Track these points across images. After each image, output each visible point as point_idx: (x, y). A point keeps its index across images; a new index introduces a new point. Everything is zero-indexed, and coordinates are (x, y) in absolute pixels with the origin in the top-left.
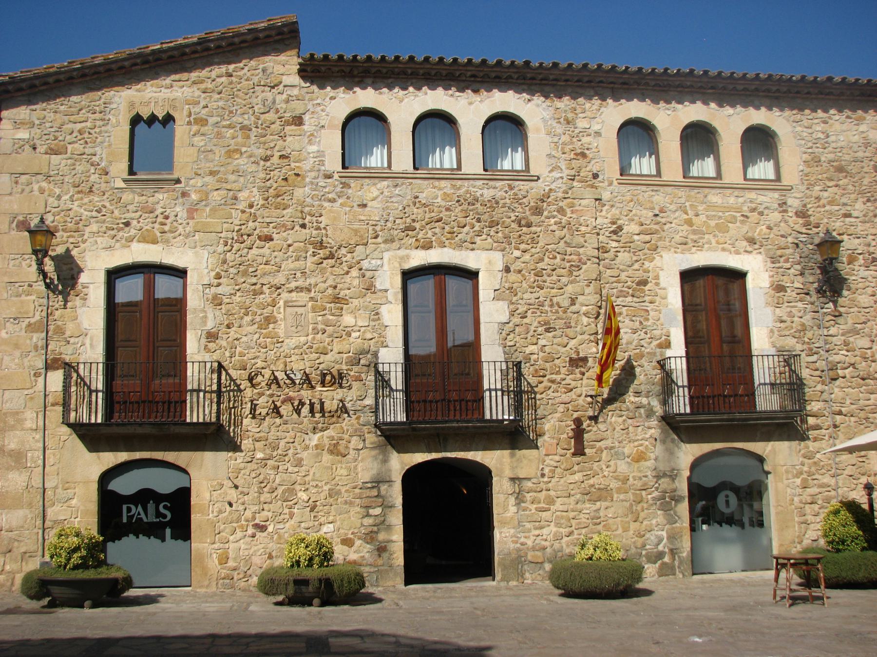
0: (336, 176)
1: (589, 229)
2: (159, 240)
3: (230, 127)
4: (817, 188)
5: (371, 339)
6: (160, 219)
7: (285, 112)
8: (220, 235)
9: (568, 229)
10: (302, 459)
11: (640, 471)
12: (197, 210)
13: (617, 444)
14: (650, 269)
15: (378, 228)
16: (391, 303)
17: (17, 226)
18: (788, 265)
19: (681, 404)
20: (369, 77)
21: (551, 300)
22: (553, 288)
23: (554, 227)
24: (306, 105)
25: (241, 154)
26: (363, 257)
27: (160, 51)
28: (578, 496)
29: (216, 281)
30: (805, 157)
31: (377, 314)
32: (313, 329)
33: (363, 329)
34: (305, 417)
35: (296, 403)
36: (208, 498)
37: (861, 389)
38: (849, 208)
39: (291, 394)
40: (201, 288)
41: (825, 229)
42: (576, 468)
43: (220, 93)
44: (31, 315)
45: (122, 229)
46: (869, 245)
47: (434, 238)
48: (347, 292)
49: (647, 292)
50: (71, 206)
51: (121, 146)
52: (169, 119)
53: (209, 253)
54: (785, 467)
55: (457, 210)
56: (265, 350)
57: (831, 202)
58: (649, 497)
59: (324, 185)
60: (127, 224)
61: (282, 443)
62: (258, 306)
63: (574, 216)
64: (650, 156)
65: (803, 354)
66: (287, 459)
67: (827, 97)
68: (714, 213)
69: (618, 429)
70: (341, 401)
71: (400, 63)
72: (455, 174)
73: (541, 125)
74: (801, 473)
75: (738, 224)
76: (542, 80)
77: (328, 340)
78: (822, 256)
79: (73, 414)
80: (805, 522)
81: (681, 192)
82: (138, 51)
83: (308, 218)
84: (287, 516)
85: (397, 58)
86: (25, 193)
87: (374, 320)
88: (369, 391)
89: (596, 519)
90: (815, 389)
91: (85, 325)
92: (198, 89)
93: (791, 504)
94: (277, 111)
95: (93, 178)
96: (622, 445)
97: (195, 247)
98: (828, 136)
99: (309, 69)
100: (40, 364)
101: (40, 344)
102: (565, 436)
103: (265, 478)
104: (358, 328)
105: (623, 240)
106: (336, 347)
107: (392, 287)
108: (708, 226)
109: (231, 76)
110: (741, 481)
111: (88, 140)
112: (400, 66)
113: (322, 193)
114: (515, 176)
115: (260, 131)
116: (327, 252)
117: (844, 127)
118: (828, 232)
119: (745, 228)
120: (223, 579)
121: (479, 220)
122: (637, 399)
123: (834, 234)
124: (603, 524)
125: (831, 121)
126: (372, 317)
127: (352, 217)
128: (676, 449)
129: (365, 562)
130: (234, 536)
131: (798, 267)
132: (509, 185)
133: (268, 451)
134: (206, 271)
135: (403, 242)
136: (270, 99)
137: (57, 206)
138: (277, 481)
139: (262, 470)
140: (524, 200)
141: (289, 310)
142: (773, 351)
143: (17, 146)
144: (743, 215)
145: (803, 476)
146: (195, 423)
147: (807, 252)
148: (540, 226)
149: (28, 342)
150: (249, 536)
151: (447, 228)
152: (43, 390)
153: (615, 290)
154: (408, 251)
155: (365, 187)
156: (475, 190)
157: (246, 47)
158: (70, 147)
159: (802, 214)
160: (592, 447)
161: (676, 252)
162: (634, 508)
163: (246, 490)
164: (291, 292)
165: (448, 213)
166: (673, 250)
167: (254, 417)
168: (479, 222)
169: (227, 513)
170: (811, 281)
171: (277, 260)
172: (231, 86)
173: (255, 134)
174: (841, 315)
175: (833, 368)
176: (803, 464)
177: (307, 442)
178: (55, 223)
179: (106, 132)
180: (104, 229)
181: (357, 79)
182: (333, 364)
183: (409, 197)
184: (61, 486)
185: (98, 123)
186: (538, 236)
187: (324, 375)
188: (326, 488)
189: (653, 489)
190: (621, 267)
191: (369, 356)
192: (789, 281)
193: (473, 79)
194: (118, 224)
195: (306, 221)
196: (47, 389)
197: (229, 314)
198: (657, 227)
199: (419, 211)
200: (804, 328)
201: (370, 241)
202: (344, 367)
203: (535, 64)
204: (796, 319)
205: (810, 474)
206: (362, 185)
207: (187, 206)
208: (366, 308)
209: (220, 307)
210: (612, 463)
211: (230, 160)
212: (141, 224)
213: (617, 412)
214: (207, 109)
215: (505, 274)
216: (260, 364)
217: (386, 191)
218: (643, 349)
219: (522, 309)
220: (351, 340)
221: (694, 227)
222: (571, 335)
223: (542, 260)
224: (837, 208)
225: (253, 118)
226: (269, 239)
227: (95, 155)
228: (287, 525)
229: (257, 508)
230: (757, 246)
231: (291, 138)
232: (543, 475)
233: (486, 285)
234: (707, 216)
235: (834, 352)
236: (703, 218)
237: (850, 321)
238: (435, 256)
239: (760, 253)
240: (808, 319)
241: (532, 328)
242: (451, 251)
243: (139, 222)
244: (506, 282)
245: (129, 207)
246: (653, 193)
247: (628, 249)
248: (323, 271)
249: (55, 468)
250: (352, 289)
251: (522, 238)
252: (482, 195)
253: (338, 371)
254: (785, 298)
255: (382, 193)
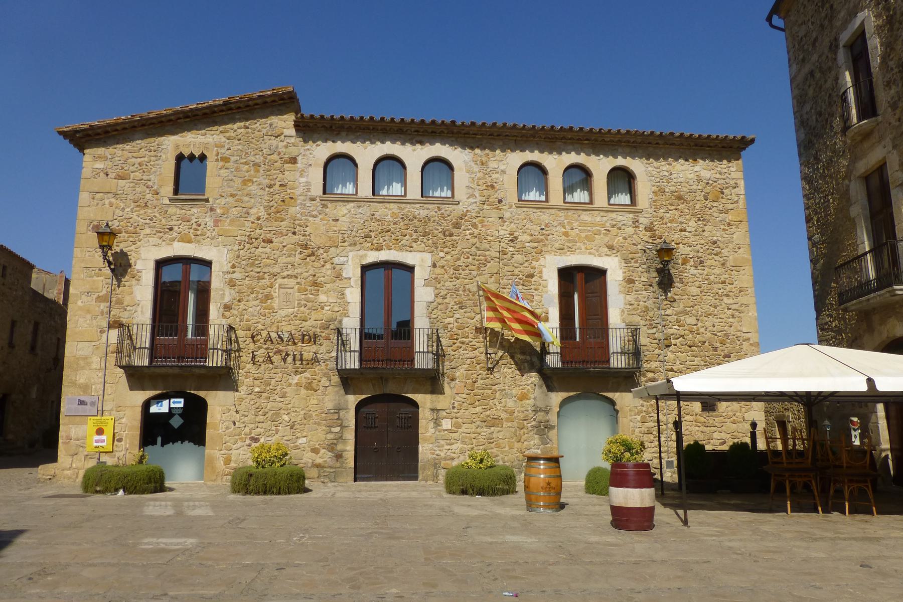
0: (318, 200)
1: (494, 238)
2: (193, 240)
3: (246, 163)
4: (662, 211)
6: (194, 226)
7: (284, 154)
8: (236, 238)
9: (479, 238)
11: (523, 407)
12: (220, 221)
13: (507, 387)
14: (536, 266)
15: (346, 236)
16: (353, 287)
17: (93, 228)
18: (637, 265)
21: (464, 287)
22: (466, 279)
23: (469, 237)
24: (300, 150)
25: (253, 183)
26: (334, 255)
27: (197, 109)
28: (478, 423)
30: (654, 188)
31: (343, 294)
32: (298, 304)
33: (332, 305)
34: (290, 363)
35: (284, 354)
36: (219, 419)
37: (688, 354)
38: (684, 225)
42: (477, 403)
43: (239, 140)
45: (167, 232)
46: (698, 252)
47: (384, 244)
49: (533, 283)
50: (131, 216)
52: (203, 157)
54: (629, 408)
57: (671, 221)
58: (529, 425)
59: (310, 205)
61: (273, 382)
62: (261, 288)
64: (536, 192)
66: (276, 392)
67: (671, 146)
68: (584, 228)
69: (508, 377)
70: (315, 353)
72: (400, 200)
76: (465, 134)
81: (561, 213)
82: (180, 109)
83: (298, 227)
84: (274, 432)
85: (362, 118)
89: (490, 440)
90: (654, 353)
96: (510, 388)
98: (671, 174)
99: (301, 125)
100: (105, 324)
103: (260, 405)
108: (580, 237)
111: (145, 170)
112: (364, 123)
114: (444, 201)
115: (266, 167)
116: (310, 251)
119: (607, 239)
121: (416, 232)
124: (495, 443)
129: (326, 465)
131: (645, 266)
133: (263, 387)
135: (363, 245)
138: (268, 408)
142: (623, 325)
144: (606, 230)
149: (97, 309)
151: (394, 237)
153: (510, 281)
154: (366, 252)
155: (338, 207)
156: (414, 210)
157: (259, 108)
158: (132, 175)
159: (649, 229)
161: (555, 255)
162: (518, 432)
163: (246, 414)
165: (395, 226)
166: (553, 253)
167: (254, 364)
168: (416, 233)
169: (232, 429)
171: (275, 256)
172: (247, 135)
173: (263, 169)
174: (675, 301)
177: (291, 381)
178: (120, 227)
180: (154, 232)
181: (335, 132)
183: (368, 215)
184: (115, 409)
185: (153, 158)
186: (457, 243)
187: (304, 336)
188: (302, 412)
189: (532, 420)
190: (515, 265)
191: (336, 323)
192: (637, 276)
193: (416, 133)
195: (296, 230)
198: (542, 237)
199: (375, 224)
200: (647, 309)
201: (340, 244)
203: (459, 123)
204: (641, 303)
207: (214, 218)
210: (503, 400)
211: (245, 187)
212: (180, 229)
213: (508, 365)
216: (260, 327)
217: (352, 210)
219: (443, 293)
220: (324, 312)
221: (570, 238)
223: (459, 259)
224: (675, 225)
227: (150, 181)
230: (614, 251)
231: (288, 172)
232: (454, 408)
233: (420, 276)
234: (580, 230)
236: (577, 231)
237: (682, 305)
239: (617, 256)
240: (650, 303)
241: (450, 306)
242: (395, 252)
243: (179, 228)
244: (433, 274)
245: (172, 217)
246: (541, 214)
248: (306, 264)
250: (326, 277)
252: (419, 214)
253: (314, 332)
254: (634, 288)
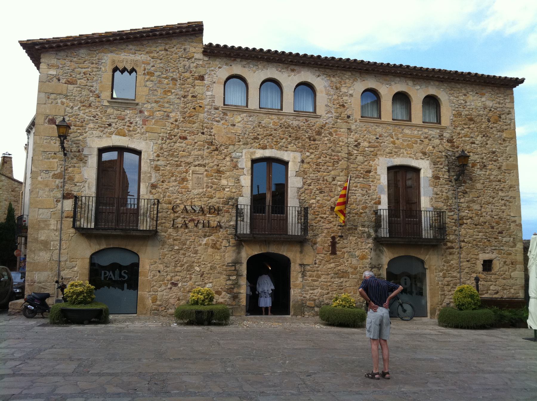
0: (220, 109)
2: (127, 135)
3: (166, 78)
4: (459, 128)
5: (235, 192)
6: (128, 124)
7: (195, 73)
10: (198, 250)
13: (352, 250)
14: (373, 165)
17: (49, 121)
18: (442, 166)
19: (384, 232)
20: (239, 58)
21: (323, 178)
22: (324, 172)
23: (326, 142)
28: (332, 275)
29: (157, 158)
31: (238, 180)
32: (206, 186)
33: (231, 187)
34: (201, 229)
35: (196, 222)
38: (474, 139)
39: (194, 217)
40: (149, 161)
41: (462, 149)
42: (332, 261)
44: (55, 169)
45: (107, 127)
47: (268, 144)
48: (224, 168)
50: (79, 113)
51: (107, 83)
53: (154, 144)
55: (280, 131)
56: (181, 195)
57: (465, 136)
59: (214, 113)
60: (110, 125)
61: (188, 242)
62: (178, 172)
63: (337, 137)
65: (447, 211)
69: (353, 243)
70: (219, 222)
71: (255, 52)
73: (324, 89)
74: (443, 270)
75: (418, 145)
76: (325, 66)
77: (213, 192)
78: (459, 163)
79: (78, 223)
80: (444, 294)
83: (206, 129)
84: (189, 279)
86: (53, 104)
87: (236, 183)
88: (233, 218)
89: (340, 287)
91: (86, 176)
92: (149, 56)
93: (437, 285)
94: (191, 72)
95: (91, 99)
96: (355, 251)
97: (146, 140)
100: (60, 195)
101: (60, 185)
102: (327, 245)
103: (179, 259)
104: (228, 187)
105: (360, 150)
106: (217, 196)
107: (246, 167)
108: (403, 145)
109: (167, 51)
110: (413, 273)
111: (89, 78)
113: (213, 117)
116: (214, 147)
117: (475, 98)
118: (463, 151)
119: (421, 147)
120: (154, 310)
121: (290, 136)
122: (363, 229)
123: (466, 152)
125: (468, 95)
126: (236, 181)
127: (227, 130)
128: (381, 254)
130: (161, 288)
132: (306, 120)
133: (180, 246)
134: (152, 153)
135: (253, 145)
136: (188, 65)
137: (71, 112)
139: (177, 255)
140: (313, 128)
141: (194, 175)
142: (431, 209)
143: (49, 78)
144: (420, 140)
145: (443, 272)
146: (144, 230)
147: (451, 160)
148: (320, 141)
149: (53, 183)
150: (168, 289)
151: (275, 140)
152: (61, 209)
153: (355, 175)
154: (255, 150)
155: (235, 116)
159: (450, 141)
160: (340, 251)
161: (386, 157)
164: (195, 166)
165: (275, 132)
166: (384, 156)
170: (453, 175)
171: (189, 150)
173: (179, 83)
175: (462, 218)
176: (444, 266)
178: (70, 122)
179: (99, 75)
180: (97, 127)
181: (232, 59)
182: (215, 204)
183: (256, 123)
184: (69, 260)
185: (95, 70)
187: (210, 209)
190: (358, 163)
191: (233, 200)
194: (105, 124)
195: (204, 131)
196: (63, 209)
197: (163, 175)
198: (377, 144)
200: (448, 198)
202: (221, 205)
205: (447, 271)
206: (233, 114)
208: (233, 177)
209: (158, 172)
210: (350, 259)
211: (166, 96)
214: (154, 68)
215: (302, 164)
218: (367, 204)
219: (309, 182)
220: (225, 192)
222: (332, 195)
223: (320, 158)
224: (468, 139)
225: (178, 75)
226: (185, 138)
228: (188, 283)
229: (173, 274)
230: (427, 156)
232: (315, 263)
233: (291, 166)
234: (403, 140)
235: (462, 211)
236: (401, 141)
238: (268, 153)
242: (276, 151)
243: (116, 124)
245: (111, 116)
246: (377, 127)
247: (362, 155)
248: (212, 157)
249: (66, 250)
251: (311, 146)
252: (292, 124)
255: (243, 120)
